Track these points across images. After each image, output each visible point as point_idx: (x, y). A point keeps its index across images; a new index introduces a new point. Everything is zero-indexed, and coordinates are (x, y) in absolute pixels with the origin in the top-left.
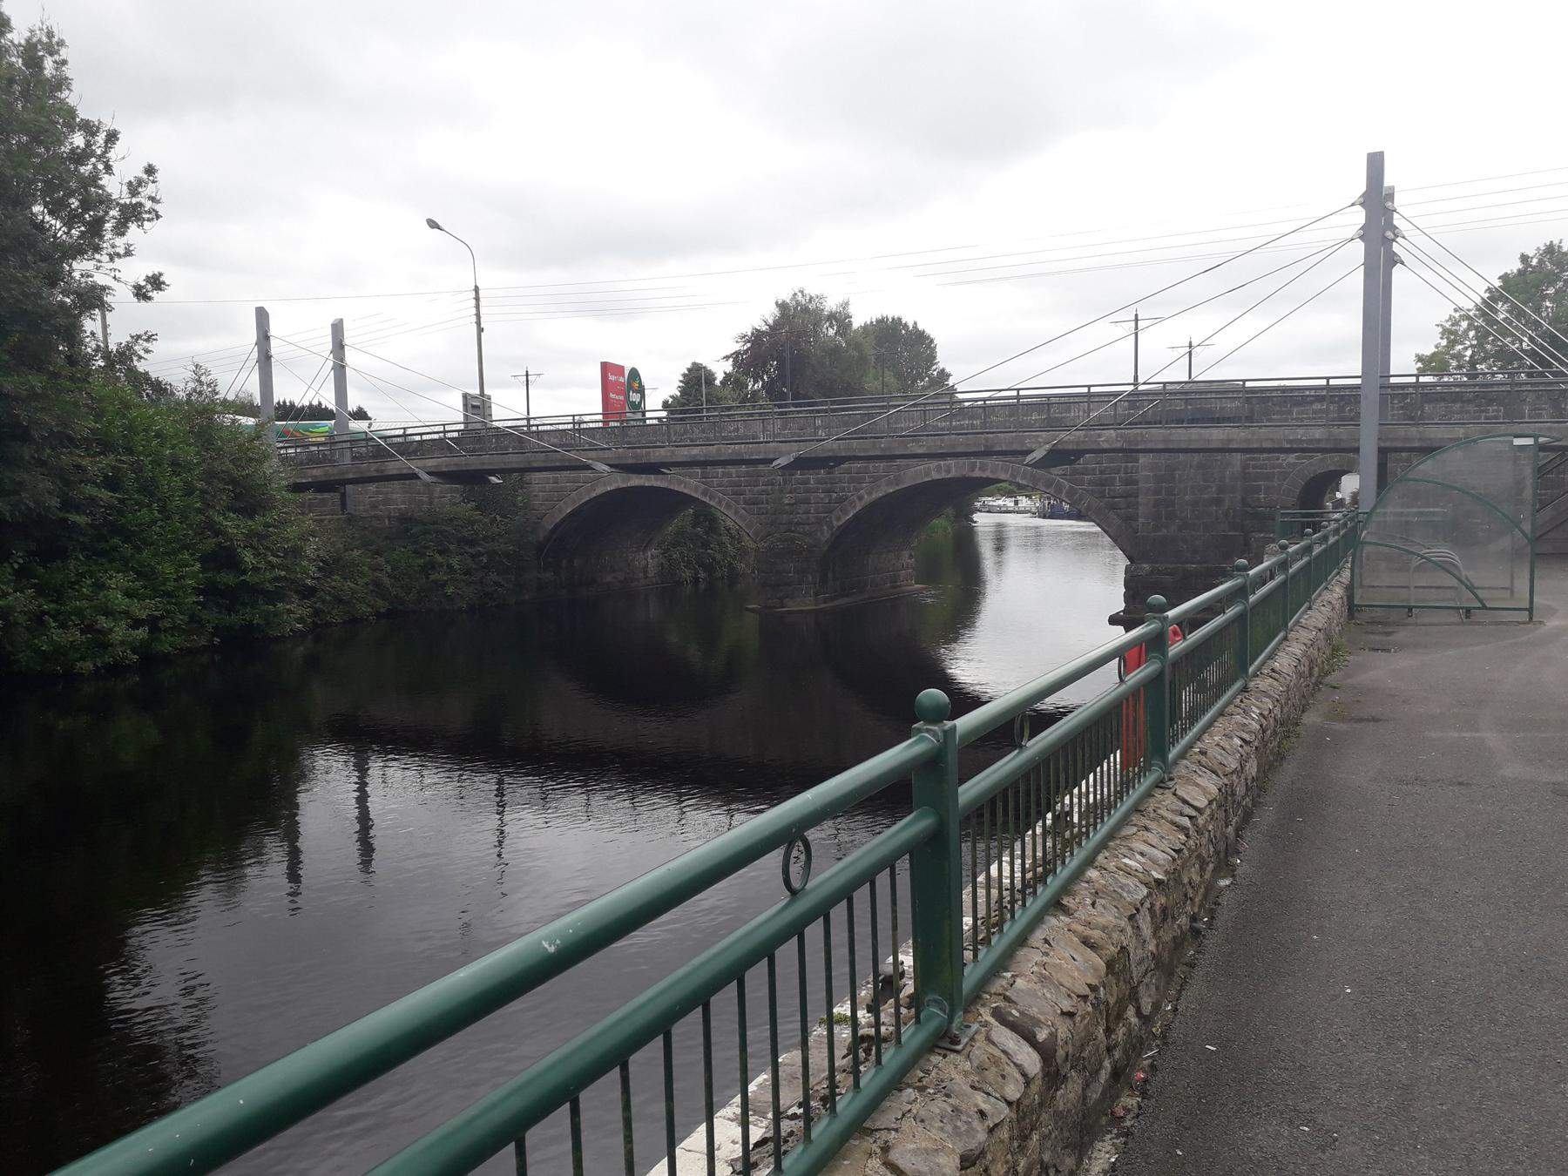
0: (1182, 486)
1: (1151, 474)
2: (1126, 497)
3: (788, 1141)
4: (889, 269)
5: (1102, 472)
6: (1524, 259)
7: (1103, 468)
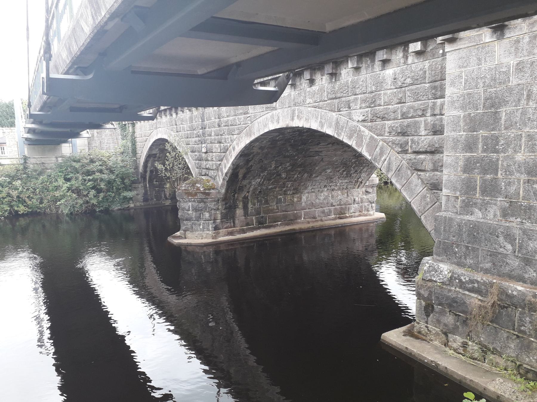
0: (512, 133)
1: (461, 114)
2: (432, 153)
3: (494, 348)
4: (28, 38)
5: (404, 116)
6: (54, 365)
7: (405, 110)
